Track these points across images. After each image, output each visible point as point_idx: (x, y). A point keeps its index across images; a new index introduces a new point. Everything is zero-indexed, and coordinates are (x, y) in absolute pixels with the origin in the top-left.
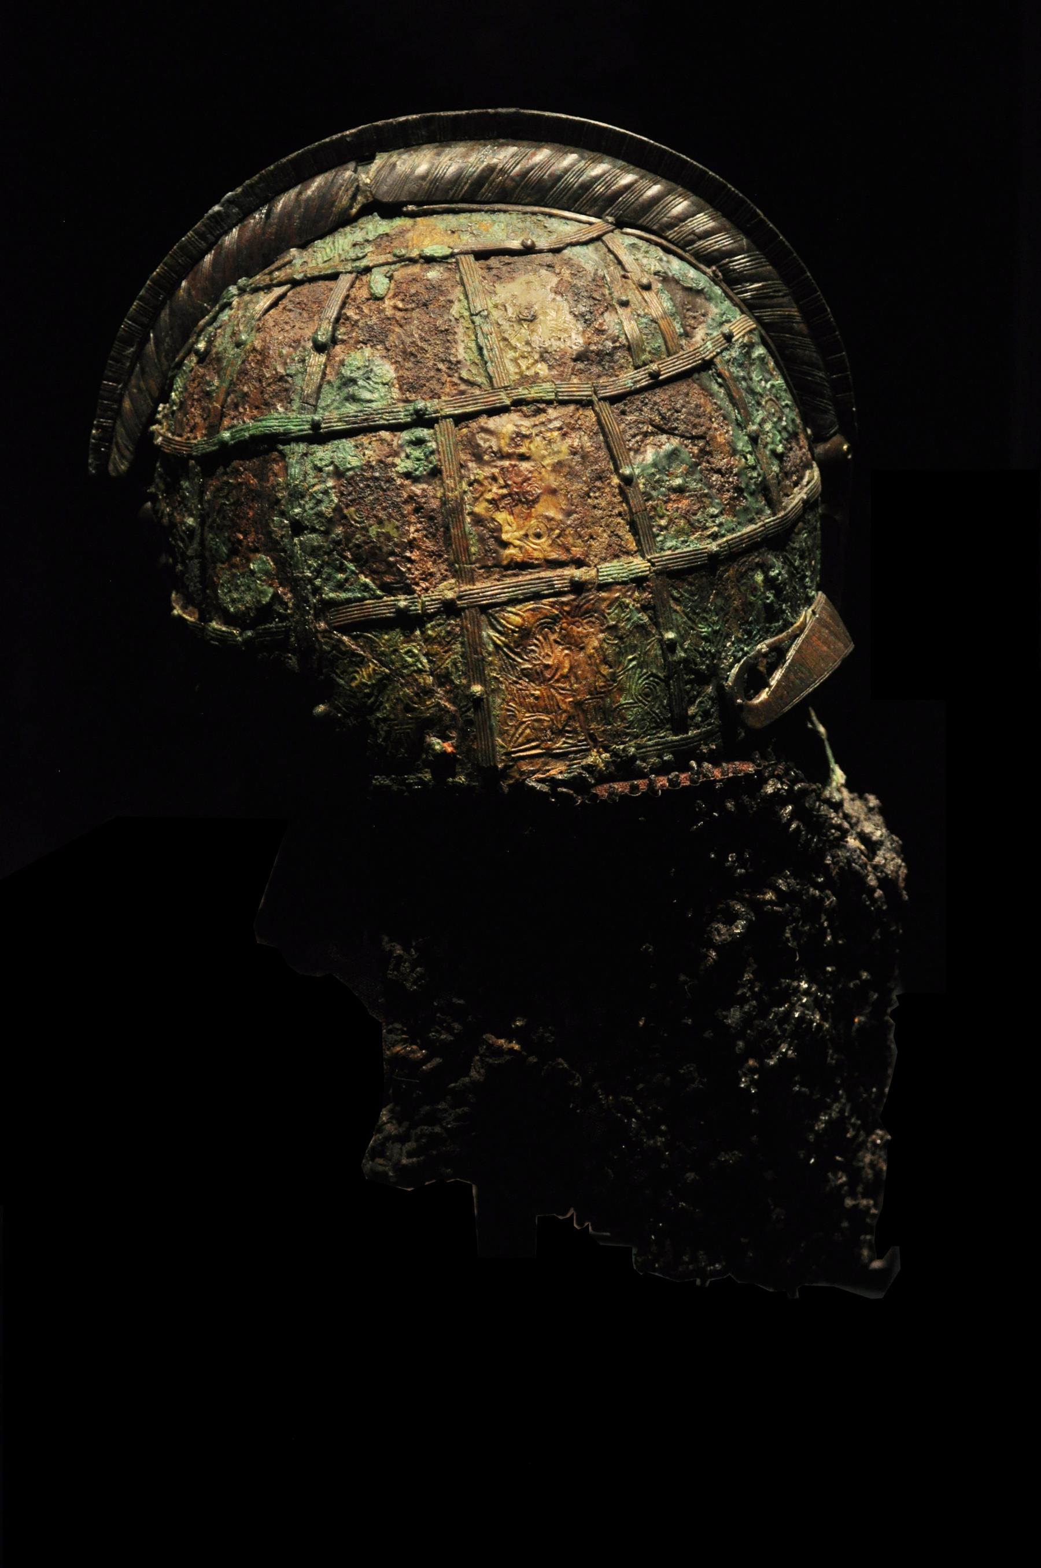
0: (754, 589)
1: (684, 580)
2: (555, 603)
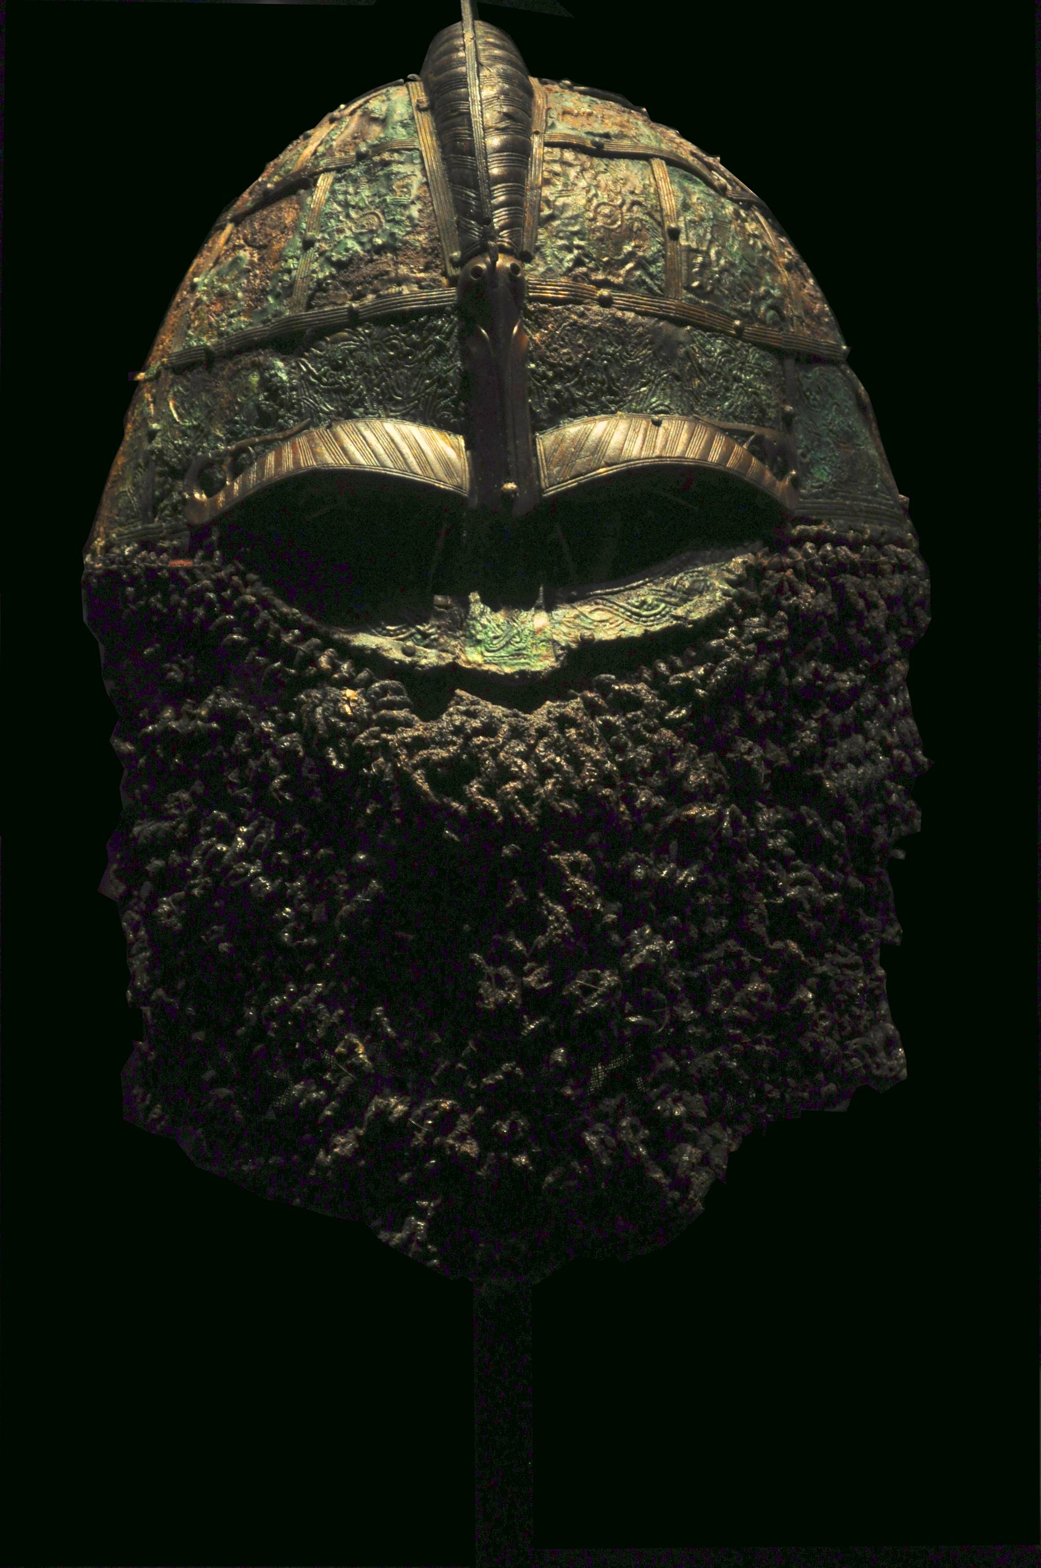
0: (247, 389)
1: (185, 376)
2: (653, 609)
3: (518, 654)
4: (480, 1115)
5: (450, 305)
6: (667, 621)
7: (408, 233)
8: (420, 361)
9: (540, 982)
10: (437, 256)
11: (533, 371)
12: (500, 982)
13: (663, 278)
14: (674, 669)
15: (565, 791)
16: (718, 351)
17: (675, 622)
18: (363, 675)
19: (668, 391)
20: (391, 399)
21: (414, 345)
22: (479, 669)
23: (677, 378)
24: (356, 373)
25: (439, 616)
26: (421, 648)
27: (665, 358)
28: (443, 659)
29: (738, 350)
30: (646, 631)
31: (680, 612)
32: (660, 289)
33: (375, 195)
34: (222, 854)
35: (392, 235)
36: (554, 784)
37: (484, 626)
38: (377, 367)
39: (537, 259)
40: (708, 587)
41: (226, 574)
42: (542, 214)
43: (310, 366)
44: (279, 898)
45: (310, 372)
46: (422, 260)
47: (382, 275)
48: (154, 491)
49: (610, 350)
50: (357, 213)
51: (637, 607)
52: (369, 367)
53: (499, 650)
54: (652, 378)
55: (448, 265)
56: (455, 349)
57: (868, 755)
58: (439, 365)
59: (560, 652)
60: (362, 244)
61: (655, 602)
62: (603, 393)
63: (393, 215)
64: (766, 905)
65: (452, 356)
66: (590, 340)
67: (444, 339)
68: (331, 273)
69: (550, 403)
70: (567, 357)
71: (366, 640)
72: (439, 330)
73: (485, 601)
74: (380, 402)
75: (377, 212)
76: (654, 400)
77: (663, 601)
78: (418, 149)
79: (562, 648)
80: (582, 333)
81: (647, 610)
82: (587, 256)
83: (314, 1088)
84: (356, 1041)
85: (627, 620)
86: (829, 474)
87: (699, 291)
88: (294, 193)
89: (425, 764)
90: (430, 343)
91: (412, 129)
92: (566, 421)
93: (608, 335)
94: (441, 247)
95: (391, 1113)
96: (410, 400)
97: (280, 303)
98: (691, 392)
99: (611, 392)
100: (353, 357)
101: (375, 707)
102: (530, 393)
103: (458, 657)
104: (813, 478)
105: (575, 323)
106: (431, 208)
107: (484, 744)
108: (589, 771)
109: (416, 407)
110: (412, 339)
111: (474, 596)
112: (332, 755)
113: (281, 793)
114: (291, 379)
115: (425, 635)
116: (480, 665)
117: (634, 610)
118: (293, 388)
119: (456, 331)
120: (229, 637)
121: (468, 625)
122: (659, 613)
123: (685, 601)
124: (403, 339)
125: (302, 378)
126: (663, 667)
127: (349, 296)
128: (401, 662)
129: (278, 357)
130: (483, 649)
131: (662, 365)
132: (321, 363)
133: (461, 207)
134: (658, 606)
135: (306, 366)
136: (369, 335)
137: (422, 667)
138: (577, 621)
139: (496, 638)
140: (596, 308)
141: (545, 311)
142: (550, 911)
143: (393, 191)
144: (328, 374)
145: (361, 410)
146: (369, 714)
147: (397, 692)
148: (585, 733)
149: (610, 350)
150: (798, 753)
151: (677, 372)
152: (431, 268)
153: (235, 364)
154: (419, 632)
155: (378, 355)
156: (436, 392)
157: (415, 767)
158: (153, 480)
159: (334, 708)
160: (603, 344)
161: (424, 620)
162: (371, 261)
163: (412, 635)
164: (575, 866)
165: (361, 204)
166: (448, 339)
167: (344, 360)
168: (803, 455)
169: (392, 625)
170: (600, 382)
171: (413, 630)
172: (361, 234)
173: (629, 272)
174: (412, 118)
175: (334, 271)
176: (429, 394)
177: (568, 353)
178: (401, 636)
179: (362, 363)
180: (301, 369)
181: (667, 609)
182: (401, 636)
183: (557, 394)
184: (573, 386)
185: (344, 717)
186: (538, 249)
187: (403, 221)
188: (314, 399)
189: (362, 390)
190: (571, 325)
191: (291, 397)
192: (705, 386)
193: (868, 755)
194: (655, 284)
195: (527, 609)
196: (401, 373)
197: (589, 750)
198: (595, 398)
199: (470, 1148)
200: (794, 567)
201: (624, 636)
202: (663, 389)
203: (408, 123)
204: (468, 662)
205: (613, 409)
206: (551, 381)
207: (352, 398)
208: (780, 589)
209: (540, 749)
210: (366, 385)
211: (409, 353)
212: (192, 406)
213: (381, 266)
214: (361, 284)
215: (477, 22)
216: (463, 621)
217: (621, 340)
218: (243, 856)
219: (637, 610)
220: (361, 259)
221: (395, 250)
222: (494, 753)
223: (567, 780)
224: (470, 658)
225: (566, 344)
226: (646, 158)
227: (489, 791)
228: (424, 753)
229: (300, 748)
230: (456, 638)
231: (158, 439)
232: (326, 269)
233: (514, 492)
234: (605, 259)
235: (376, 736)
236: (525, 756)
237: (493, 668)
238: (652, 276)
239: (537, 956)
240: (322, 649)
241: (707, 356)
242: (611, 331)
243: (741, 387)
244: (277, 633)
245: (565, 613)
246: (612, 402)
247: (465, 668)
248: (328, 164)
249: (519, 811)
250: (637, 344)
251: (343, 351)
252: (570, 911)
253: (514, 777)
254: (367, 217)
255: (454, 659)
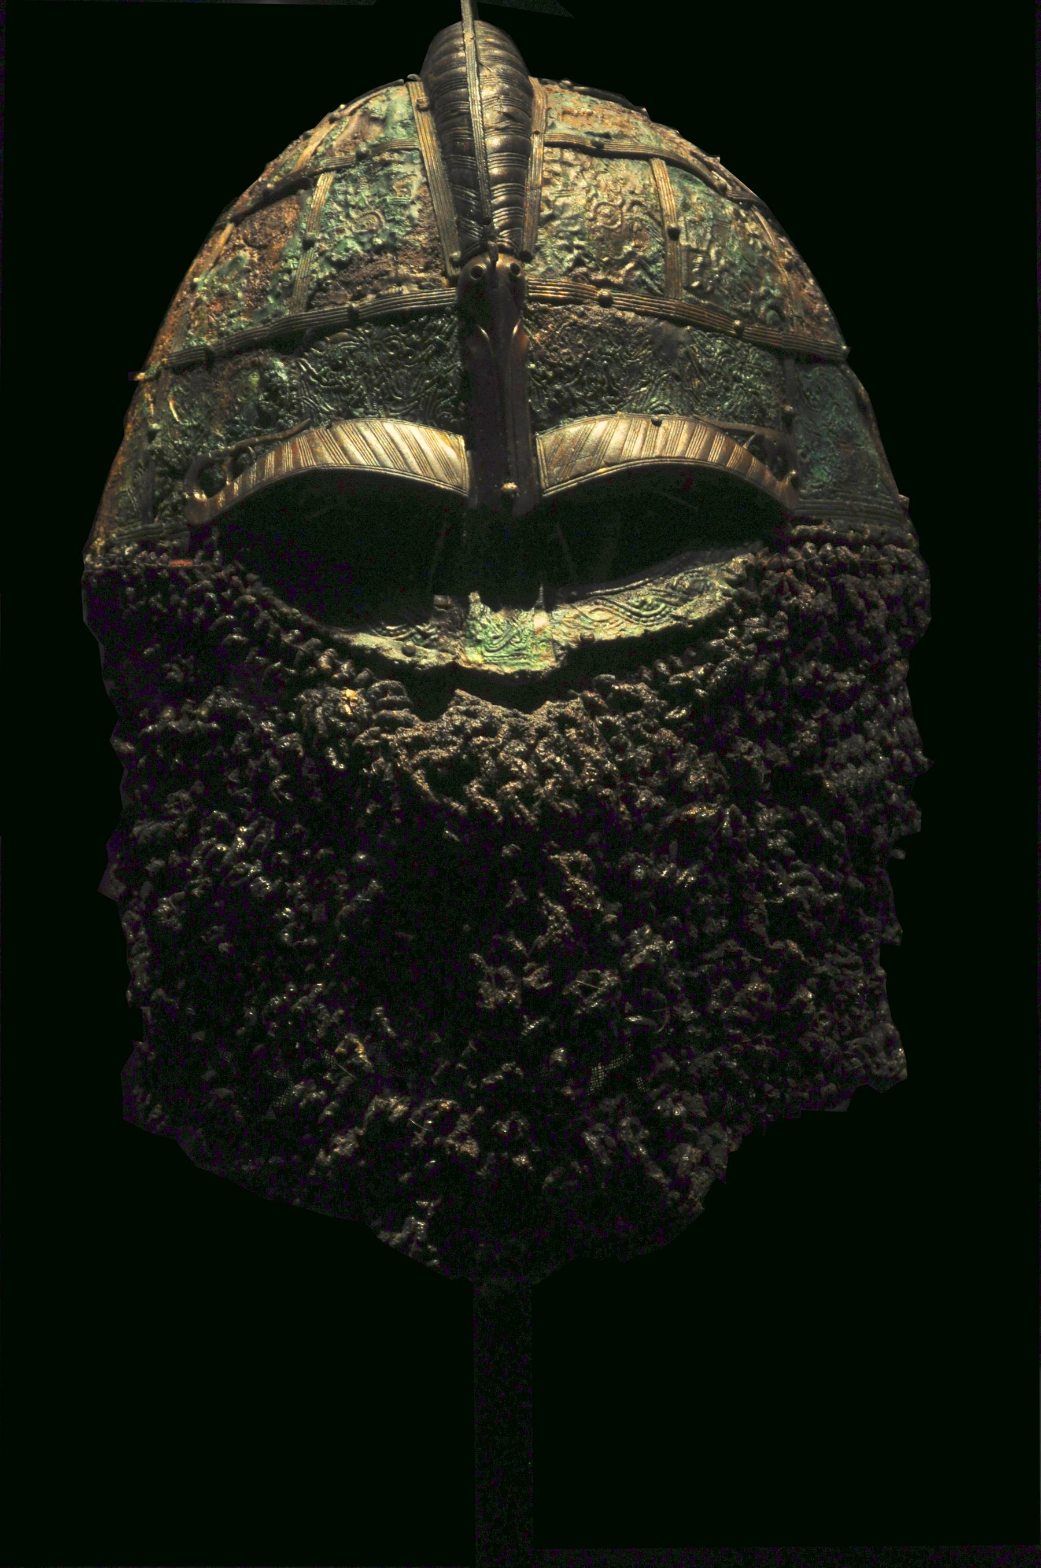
0: (247, 389)
1: (185, 376)
2: (653, 609)
3: (518, 654)
4: (480, 1115)
5: (450, 305)
6: (667, 621)
7: (408, 233)
8: (420, 361)
9: (540, 982)
10: (437, 256)
11: (533, 371)
12: (500, 982)
13: (663, 278)
14: (674, 669)
15: (565, 791)
16: (718, 351)
17: (675, 622)
18: (363, 675)
19: (668, 391)
20: (391, 399)
21: (414, 345)
22: (479, 669)
23: (677, 378)
24: (356, 373)
25: (439, 616)
26: (421, 648)
27: (665, 358)
28: (443, 659)
29: (738, 350)
30: (646, 631)
31: (680, 612)
32: (660, 289)
33: (375, 195)
34: (222, 854)
35: (392, 235)
36: (554, 784)
37: (484, 626)
38: (377, 367)
39: (537, 259)
40: (708, 587)
41: (226, 574)
42: (542, 214)
43: (310, 366)
44: (279, 898)
45: (310, 372)
46: (422, 260)
47: (382, 275)
48: (154, 491)
49: (610, 350)
50: (357, 213)
51: (637, 607)
52: (369, 367)
53: (499, 650)
54: (652, 378)
55: (448, 265)
56: (455, 349)
57: (868, 755)
58: (439, 365)
59: (560, 652)
60: (362, 244)
61: (655, 602)
62: (603, 393)
63: (393, 215)
64: (766, 905)
65: (452, 356)
66: (590, 340)
67: (444, 339)
68: (331, 273)
69: (550, 403)
70: (567, 357)
71: (366, 640)
72: (439, 330)
73: (485, 601)
74: (380, 402)
75: (377, 212)
76: (654, 400)
77: (663, 601)
78: (418, 149)
79: (562, 648)
80: (582, 333)
81: (647, 610)
82: (587, 256)
83: (314, 1088)
84: (356, 1041)
85: (627, 620)
86: (829, 474)
87: (699, 291)
88: (294, 193)
89: (425, 764)
90: (430, 343)
91: (412, 129)
92: (566, 421)
93: (608, 335)
94: (441, 247)
95: (391, 1113)
96: (410, 400)
97: (280, 303)
98: (691, 392)
99: (611, 392)
100: (353, 357)
101: (375, 707)
102: (530, 393)
103: (458, 657)
104: (813, 478)
105: (575, 323)
106: (431, 208)
107: (484, 744)
108: (589, 771)
109: (416, 407)
110: (412, 339)
111: (474, 596)
112: (332, 755)
113: (281, 793)
114: (291, 379)
115: (425, 635)
116: (480, 665)
117: (634, 610)
118: (293, 388)
119: (456, 331)
120: (229, 637)
121: (468, 625)
122: (659, 613)
123: (685, 601)
124: (403, 339)
125: (302, 378)
126: (663, 667)
127: (349, 296)
128: (401, 662)
129: (278, 357)
130: (483, 649)
131: (662, 365)
132: (321, 363)
133: (461, 207)
134: (658, 606)
135: (306, 366)
136: (369, 335)
137: (422, 667)
138: (577, 621)
139: (496, 638)
140: (596, 308)
141: (545, 311)
142: (550, 911)
143: (393, 191)
144: (328, 374)
145: (361, 410)
146: (369, 714)
147: (397, 692)
148: (585, 733)
149: (610, 350)
150: (798, 753)
151: (677, 372)
152: (431, 268)
153: (235, 364)
154: (419, 632)
155: (378, 355)
156: (436, 392)
157: (415, 767)
158: (153, 480)
159: (334, 708)
160: (603, 344)
161: (424, 620)
162: (371, 261)
163: (412, 635)
164: (575, 866)
165: (361, 204)
166: (448, 339)
167: (344, 360)
168: (803, 455)
169: (392, 625)
170: (600, 382)
171: (413, 630)
172: (361, 234)
173: (629, 272)
174: (412, 118)
175: (334, 271)
176: (429, 394)
177: (568, 353)
178: (401, 636)
179: (362, 363)
180: (301, 369)
181: (667, 609)
182: (401, 636)
183: (557, 394)
184: (573, 386)
185: (344, 717)
186: (538, 249)
187: (403, 221)
188: (314, 399)
189: (362, 390)
190: (571, 325)
191: (291, 397)
192: (705, 386)
193: (868, 755)
194: (655, 284)
195: (527, 609)
196: (401, 373)
197: (589, 750)
198: (595, 398)
199: (470, 1148)
200: (794, 567)
201: (624, 636)
202: (663, 389)
203: (408, 123)
204: (468, 662)
205: (613, 409)
206: (551, 381)
207: (352, 398)
208: (780, 589)
209: (540, 749)
210: (366, 385)
211: (409, 353)
212: (192, 406)
213: (381, 266)
214: (361, 284)
215: (477, 22)
216: (463, 621)
217: (621, 340)
218: (243, 856)
219: (637, 610)
220: (361, 259)
221: (395, 250)
222: (494, 753)
223: (567, 780)
224: (470, 658)
225: (566, 344)
226: (646, 158)
227: (489, 791)
228: (424, 753)
229: (300, 748)
230: (456, 638)
231: (158, 439)
232: (326, 269)
233: (514, 492)
234: (605, 259)
235: (376, 736)
236: (525, 756)
237: (493, 668)
238: (652, 276)
239: (537, 956)
240: (322, 649)
241: (707, 356)
242: (611, 331)
243: (741, 387)
244: (277, 633)
245: (565, 613)
246: (612, 402)
247: (465, 668)
248: (328, 164)
249: (519, 811)
250: (637, 344)
251: (343, 351)
252: (570, 911)
253: (514, 777)
254: (367, 217)
255: (454, 659)
